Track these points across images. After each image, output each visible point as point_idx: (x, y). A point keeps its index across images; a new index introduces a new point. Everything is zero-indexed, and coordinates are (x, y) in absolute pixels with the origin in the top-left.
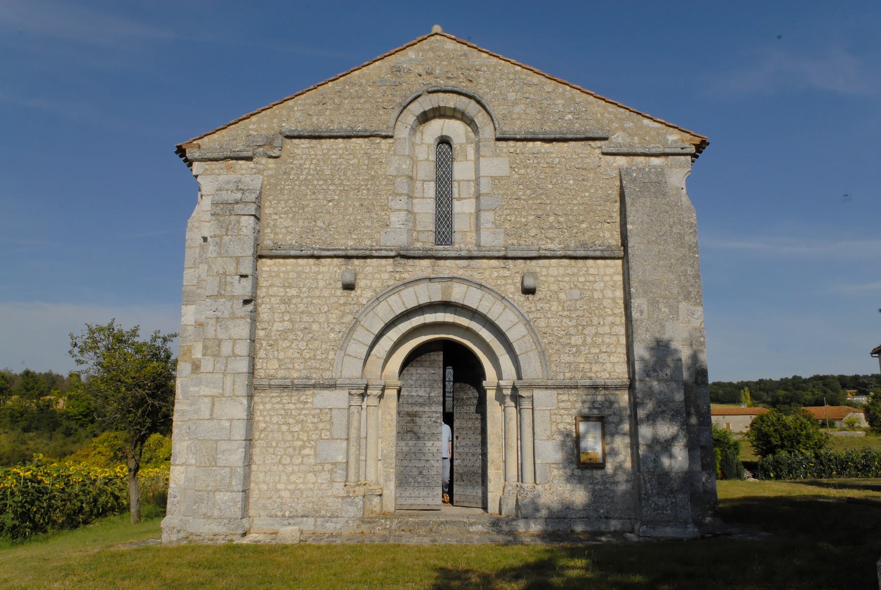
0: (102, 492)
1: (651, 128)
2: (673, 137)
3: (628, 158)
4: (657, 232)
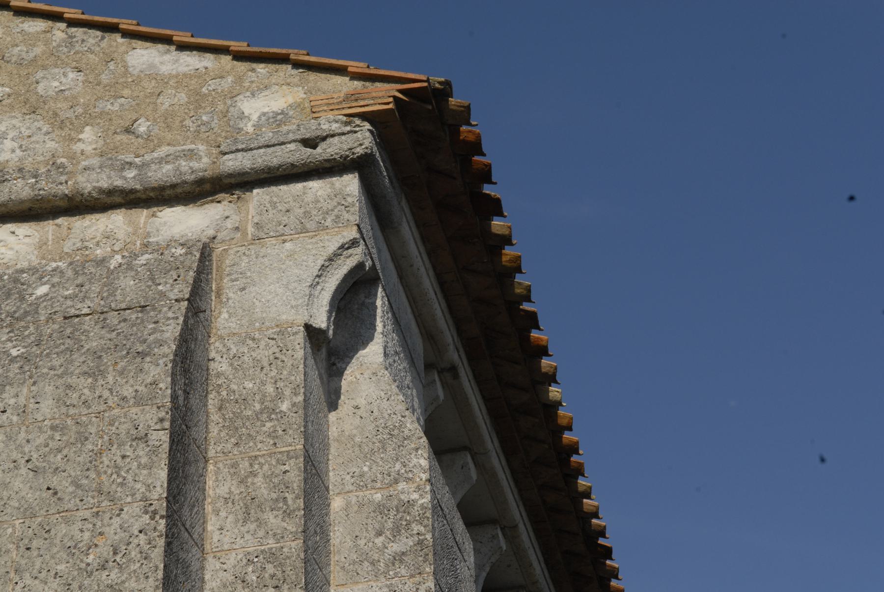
1: (163, 81)
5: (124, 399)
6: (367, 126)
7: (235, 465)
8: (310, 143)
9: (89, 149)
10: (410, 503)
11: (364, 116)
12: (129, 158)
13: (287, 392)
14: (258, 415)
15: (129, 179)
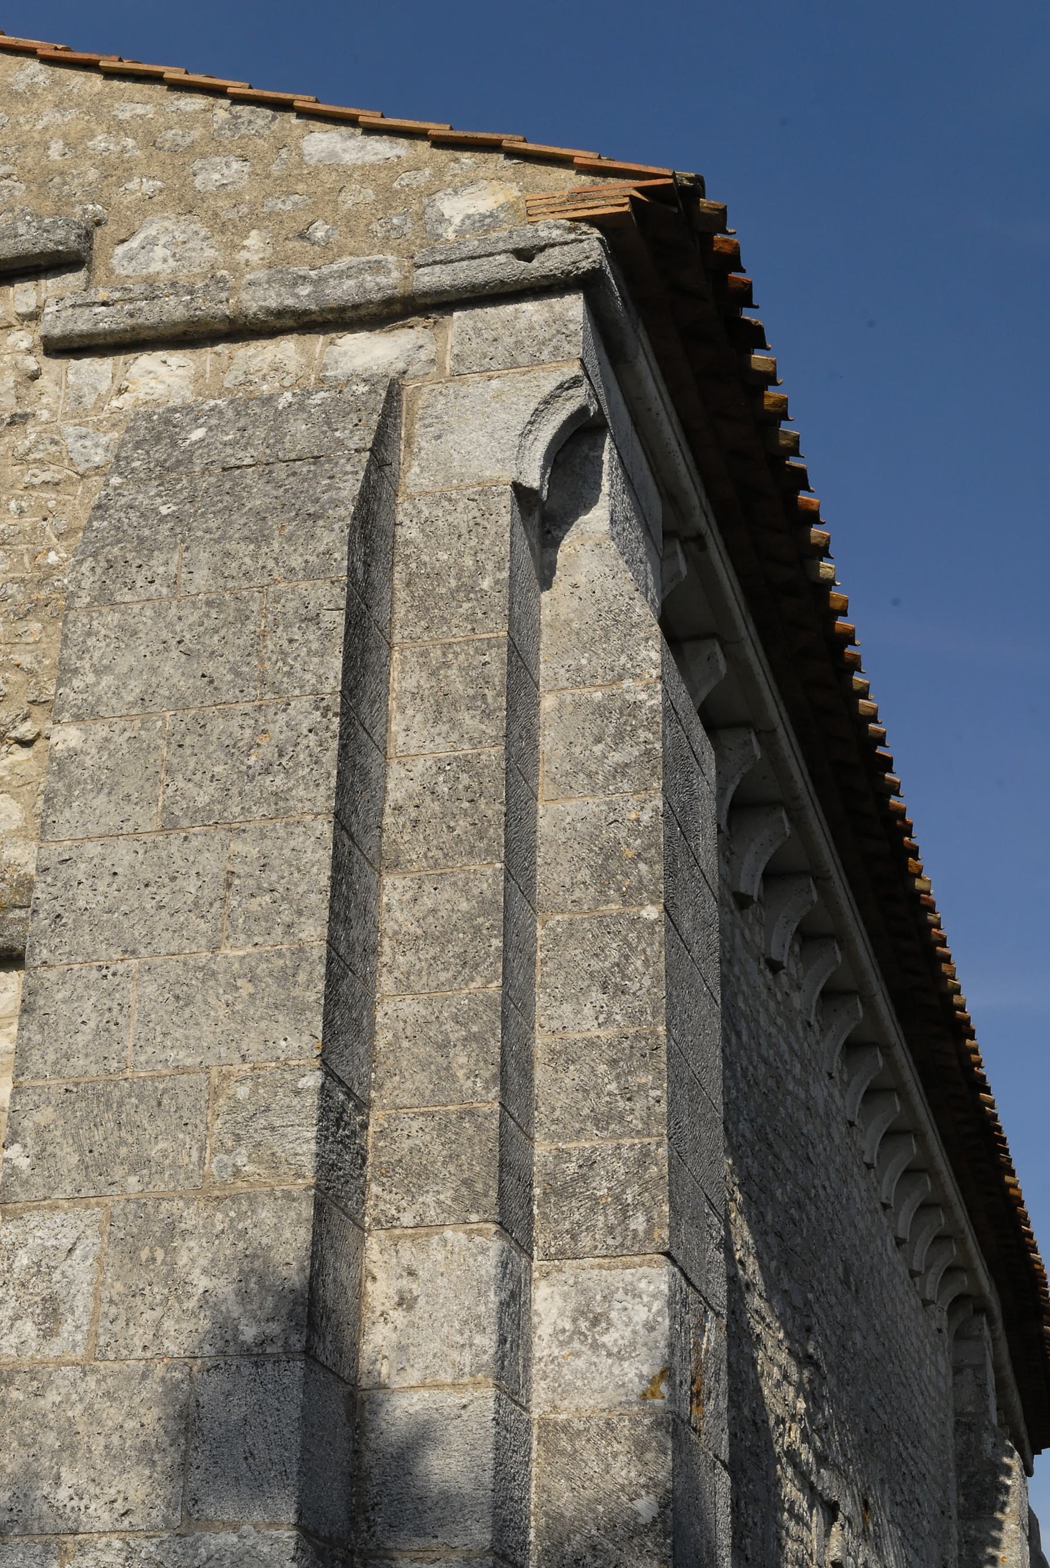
0: (164, 1427)
1: (345, 173)
2: (478, 202)
3: (207, 357)
4: (231, 749)
5: (291, 570)
6: (596, 233)
7: (425, 654)
8: (525, 254)
9: (255, 258)
10: (637, 705)
11: (592, 221)
12: (304, 270)
13: (490, 566)
14: (453, 593)
15: (302, 298)
